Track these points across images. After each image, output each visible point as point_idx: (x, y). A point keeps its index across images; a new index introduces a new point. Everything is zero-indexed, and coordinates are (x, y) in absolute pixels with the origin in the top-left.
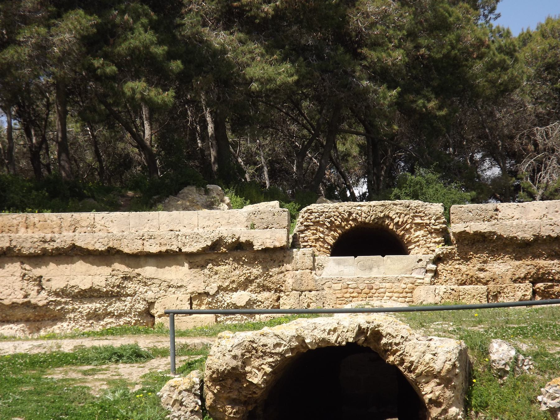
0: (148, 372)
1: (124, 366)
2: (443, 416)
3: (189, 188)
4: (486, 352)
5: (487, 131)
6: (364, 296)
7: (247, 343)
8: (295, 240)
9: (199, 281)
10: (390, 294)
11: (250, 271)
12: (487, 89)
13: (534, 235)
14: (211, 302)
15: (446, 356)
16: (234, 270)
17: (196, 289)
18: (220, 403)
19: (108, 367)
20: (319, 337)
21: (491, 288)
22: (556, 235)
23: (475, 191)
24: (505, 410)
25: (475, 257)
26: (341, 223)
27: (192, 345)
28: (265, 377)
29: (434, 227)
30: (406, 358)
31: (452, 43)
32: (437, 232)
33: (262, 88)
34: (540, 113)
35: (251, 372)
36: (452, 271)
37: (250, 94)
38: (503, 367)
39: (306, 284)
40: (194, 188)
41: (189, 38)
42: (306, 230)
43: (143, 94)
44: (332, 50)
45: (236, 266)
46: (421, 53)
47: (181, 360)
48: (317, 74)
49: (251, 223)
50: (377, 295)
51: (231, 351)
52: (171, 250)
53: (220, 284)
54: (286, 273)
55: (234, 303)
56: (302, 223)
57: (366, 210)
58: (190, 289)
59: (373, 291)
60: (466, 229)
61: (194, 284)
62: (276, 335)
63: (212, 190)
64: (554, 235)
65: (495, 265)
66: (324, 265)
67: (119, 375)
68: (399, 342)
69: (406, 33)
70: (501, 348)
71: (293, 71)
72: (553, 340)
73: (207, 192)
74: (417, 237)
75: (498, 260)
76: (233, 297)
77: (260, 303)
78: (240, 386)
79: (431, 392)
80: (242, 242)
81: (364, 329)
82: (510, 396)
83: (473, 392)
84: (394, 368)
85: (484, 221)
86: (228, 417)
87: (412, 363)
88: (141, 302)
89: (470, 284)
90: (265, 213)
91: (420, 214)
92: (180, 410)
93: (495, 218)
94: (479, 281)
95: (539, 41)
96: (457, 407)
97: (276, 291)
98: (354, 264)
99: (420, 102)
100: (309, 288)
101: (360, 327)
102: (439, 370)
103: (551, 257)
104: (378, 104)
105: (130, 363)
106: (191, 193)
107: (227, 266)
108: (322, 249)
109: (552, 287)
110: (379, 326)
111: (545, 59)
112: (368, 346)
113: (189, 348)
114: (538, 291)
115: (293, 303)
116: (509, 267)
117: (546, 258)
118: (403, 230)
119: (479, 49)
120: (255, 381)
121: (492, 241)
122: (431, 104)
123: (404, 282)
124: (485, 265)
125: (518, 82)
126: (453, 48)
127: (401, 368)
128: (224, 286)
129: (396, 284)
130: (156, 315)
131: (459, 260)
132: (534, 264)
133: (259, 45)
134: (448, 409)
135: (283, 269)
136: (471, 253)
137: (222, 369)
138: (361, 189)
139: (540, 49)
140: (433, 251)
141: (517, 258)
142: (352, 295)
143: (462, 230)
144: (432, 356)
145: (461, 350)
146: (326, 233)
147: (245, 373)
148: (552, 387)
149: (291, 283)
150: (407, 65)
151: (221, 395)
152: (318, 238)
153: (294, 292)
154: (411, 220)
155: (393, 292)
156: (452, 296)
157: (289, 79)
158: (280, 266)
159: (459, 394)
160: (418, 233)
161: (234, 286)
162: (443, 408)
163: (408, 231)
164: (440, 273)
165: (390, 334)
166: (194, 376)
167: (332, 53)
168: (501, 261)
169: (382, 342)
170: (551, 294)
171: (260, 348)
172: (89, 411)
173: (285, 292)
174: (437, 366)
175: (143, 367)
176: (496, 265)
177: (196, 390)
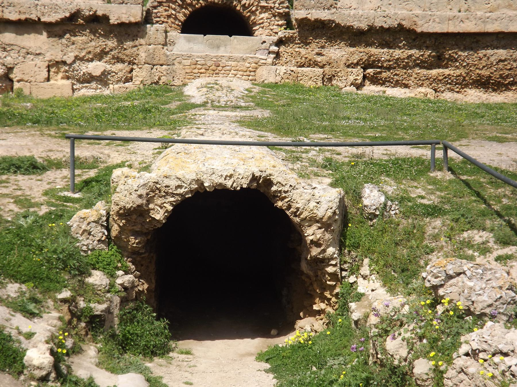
0: (48, 186)
1: (23, 178)
2: (321, 255)
4: (358, 197)
7: (151, 184)
8: (148, 15)
10: (235, 72)
11: (106, 43)
13: (368, 25)
14: (68, 71)
16: (91, 41)
17: (53, 57)
18: (125, 234)
19: (8, 179)
20: (217, 181)
21: (327, 72)
22: (388, 26)
24: (375, 252)
25: (314, 42)
28: (166, 214)
29: (278, 11)
30: (292, 204)
32: (280, 15)
35: (153, 209)
36: (292, 53)
38: (374, 211)
39: (157, 59)
42: (159, 6)
45: (93, 37)
50: (223, 72)
51: (137, 191)
52: (30, 19)
53: (77, 53)
54: (139, 47)
55: (89, 72)
58: (48, 57)
59: (220, 68)
60: (308, 16)
61: (52, 52)
64: (386, 26)
66: (176, 41)
67: (20, 189)
68: (288, 190)
74: (262, 19)
75: (335, 46)
76: (89, 66)
77: (114, 74)
79: (313, 234)
80: (99, 16)
81: (257, 177)
83: (348, 233)
84: (281, 211)
86: (131, 246)
87: (298, 209)
89: (308, 67)
92: (88, 238)
93: (335, 7)
94: (316, 64)
97: (129, 64)
100: (161, 62)
101: (253, 175)
103: (382, 46)
105: (28, 174)
107: (84, 38)
108: (173, 25)
109: (380, 73)
110: (270, 175)
113: (81, 160)
114: (368, 76)
115: (145, 76)
116: (344, 53)
117: (377, 47)
120: (158, 217)
123: (248, 61)
124: (323, 50)
127: (288, 213)
130: (14, 80)
131: (299, 44)
132: (366, 51)
135: (137, 43)
136: (311, 38)
137: (128, 206)
141: (352, 45)
142: (200, 71)
143: (304, 16)
144: (315, 204)
145: (340, 198)
146: (178, 10)
147: (149, 210)
148: (436, 268)
149: (144, 57)
151: (126, 228)
153: (146, 65)
154: (257, 3)
155: (237, 70)
156: (291, 77)
158: (133, 40)
159: (336, 236)
160: (263, 15)
161: (91, 57)
162: (322, 248)
163: (253, 13)
164: (281, 55)
165: (280, 183)
166: (100, 208)
168: (337, 47)
169: (272, 189)
170: (379, 79)
171: (163, 189)
172: (7, 240)
174: (320, 213)
177: (102, 222)
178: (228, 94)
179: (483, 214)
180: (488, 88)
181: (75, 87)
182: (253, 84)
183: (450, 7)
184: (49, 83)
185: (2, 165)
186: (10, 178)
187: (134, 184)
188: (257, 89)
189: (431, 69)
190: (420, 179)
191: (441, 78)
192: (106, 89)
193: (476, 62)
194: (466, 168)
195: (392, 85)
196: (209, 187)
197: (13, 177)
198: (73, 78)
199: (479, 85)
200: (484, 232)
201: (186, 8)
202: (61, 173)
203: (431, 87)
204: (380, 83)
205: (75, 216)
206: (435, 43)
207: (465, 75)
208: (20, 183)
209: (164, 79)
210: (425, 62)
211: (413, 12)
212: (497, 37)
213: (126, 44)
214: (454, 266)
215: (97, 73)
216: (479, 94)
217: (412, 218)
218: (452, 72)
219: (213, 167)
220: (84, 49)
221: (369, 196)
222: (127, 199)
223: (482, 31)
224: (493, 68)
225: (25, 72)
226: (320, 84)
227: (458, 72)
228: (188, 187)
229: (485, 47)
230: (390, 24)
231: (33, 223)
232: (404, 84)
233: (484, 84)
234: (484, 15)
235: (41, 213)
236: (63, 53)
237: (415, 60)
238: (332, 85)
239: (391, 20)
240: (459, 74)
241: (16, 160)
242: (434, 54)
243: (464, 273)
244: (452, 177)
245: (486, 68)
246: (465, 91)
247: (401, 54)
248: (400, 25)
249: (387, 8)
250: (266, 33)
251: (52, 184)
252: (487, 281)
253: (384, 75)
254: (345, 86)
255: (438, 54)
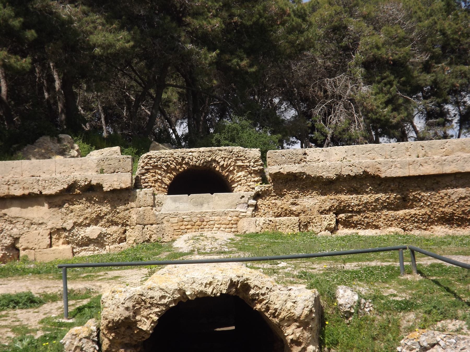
0: (44, 316)
3: (44, 137)
4: (333, 298)
5: (285, 81)
6: (197, 228)
7: (137, 296)
8: (137, 181)
9: (57, 219)
10: (219, 226)
12: (287, 49)
14: (68, 236)
15: (305, 304)
16: (87, 208)
17: (55, 225)
18: (115, 347)
19: (7, 313)
20: (197, 289)
21: (302, 219)
22: (354, 174)
23: (280, 134)
25: (288, 193)
26: (176, 167)
27: (77, 290)
28: (152, 325)
29: (253, 169)
30: (270, 306)
31: (261, 13)
32: (256, 172)
33: (104, 52)
34: (329, 66)
35: (140, 321)
36: (269, 205)
37: (94, 57)
38: (349, 310)
40: (48, 138)
41: (40, 11)
42: (147, 173)
43: (4, 61)
44: (160, 19)
45: (89, 205)
46: (235, 20)
47: (74, 304)
48: (149, 39)
49: (100, 168)
50: (207, 226)
51: (124, 303)
52: (33, 193)
53: (75, 220)
54: (131, 210)
55: (87, 236)
56: (143, 167)
57: (196, 155)
58: (50, 225)
59: (205, 223)
60: (280, 170)
61: (53, 221)
62: (161, 289)
63: (64, 139)
64: (352, 174)
65: (305, 200)
67: (18, 321)
69: (222, 4)
70: (346, 294)
71: (129, 37)
72: (383, 282)
73: (60, 141)
74: (239, 177)
75: (308, 195)
76: (87, 231)
77: (109, 236)
78: (132, 332)
79: (292, 334)
80: (93, 185)
81: (235, 282)
82: (357, 335)
84: (259, 314)
85: (295, 163)
87: (276, 310)
88: (8, 238)
89: (285, 216)
90: (112, 159)
91: (241, 158)
93: (304, 161)
94: (292, 213)
95: (327, 8)
96: (313, 345)
97: (122, 225)
98: (187, 201)
99: (235, 61)
100: (151, 222)
101: (231, 281)
102: (299, 316)
103: (351, 192)
104: (201, 64)
105: (25, 308)
106: (46, 142)
107: (81, 205)
108: (160, 188)
109: (351, 217)
110: (247, 279)
111: (332, 22)
112: (237, 295)
113: (75, 293)
114: (341, 221)
115: (137, 235)
116: (317, 201)
117: (346, 193)
118: (227, 171)
119: (282, 17)
120: (145, 328)
121: (302, 180)
122: (244, 63)
123: (230, 215)
124: (297, 200)
125: (312, 43)
126: (261, 16)
128: (79, 222)
129: (223, 217)
130: (21, 249)
131: (275, 196)
132: (336, 198)
133: (100, 16)
134: (306, 347)
135: (128, 206)
136: (285, 190)
137: (116, 319)
138: (182, 129)
139: (328, 14)
140: (253, 188)
141: (323, 194)
142: (187, 227)
143: (277, 171)
144: (292, 304)
145: (315, 298)
146: (164, 175)
147: (136, 322)
148: (410, 340)
149: (135, 219)
150: (223, 31)
151: (115, 341)
152: (157, 180)
153: (138, 225)
154: (234, 163)
155: (221, 224)
156: (270, 227)
157: (126, 45)
158: (125, 204)
159: (315, 334)
160: (240, 174)
161: (88, 222)
162: (302, 346)
163: (231, 172)
165: (257, 286)
166: (91, 325)
167: (161, 21)
168: (309, 196)
169: (250, 293)
170: (351, 223)
171: (148, 300)
173: (130, 226)
174: (297, 312)
175: (38, 312)
176: (305, 199)
177: (93, 337)
178: (213, 243)
179: (454, 305)
180: (453, 224)
181: (75, 251)
182: (236, 235)
183: (408, 153)
184: (51, 249)
185: (2, 302)
186: (10, 312)
187: (120, 298)
188: (239, 238)
189: (398, 210)
190: (391, 281)
191: (407, 218)
192: (103, 250)
193: (439, 201)
194: (434, 270)
195: (364, 227)
196: (190, 295)
197: (12, 312)
198: (73, 242)
199: (444, 222)
200: (457, 321)
201: (171, 173)
202: (56, 305)
203: (399, 226)
204: (352, 226)
205: (67, 334)
206: (399, 186)
207: (430, 213)
208: (18, 316)
209: (154, 237)
210: (392, 204)
211: (376, 160)
212: (455, 177)
213: (119, 208)
214: (427, 337)
215: (94, 236)
216: (445, 230)
217: (386, 313)
218: (417, 212)
219: (193, 277)
220: (82, 215)
221: (343, 296)
222: (115, 312)
223: (441, 172)
224: (455, 205)
225: (30, 241)
226: (297, 230)
227: (423, 211)
228: (172, 297)
229: (445, 187)
230: (356, 172)
231: (29, 344)
232: (374, 225)
233: (448, 220)
234: (440, 158)
235: (36, 337)
236: (63, 221)
237: (382, 203)
238: (308, 231)
239: (356, 168)
240: (424, 212)
241: (15, 297)
242: (399, 196)
243: (438, 344)
244: (421, 278)
245: (448, 206)
246: (432, 228)
247: (369, 198)
248: (365, 172)
249: (352, 158)
250: (244, 189)
251: (48, 314)
252: (461, 350)
253: (355, 218)
254: (321, 231)
255: (403, 196)
